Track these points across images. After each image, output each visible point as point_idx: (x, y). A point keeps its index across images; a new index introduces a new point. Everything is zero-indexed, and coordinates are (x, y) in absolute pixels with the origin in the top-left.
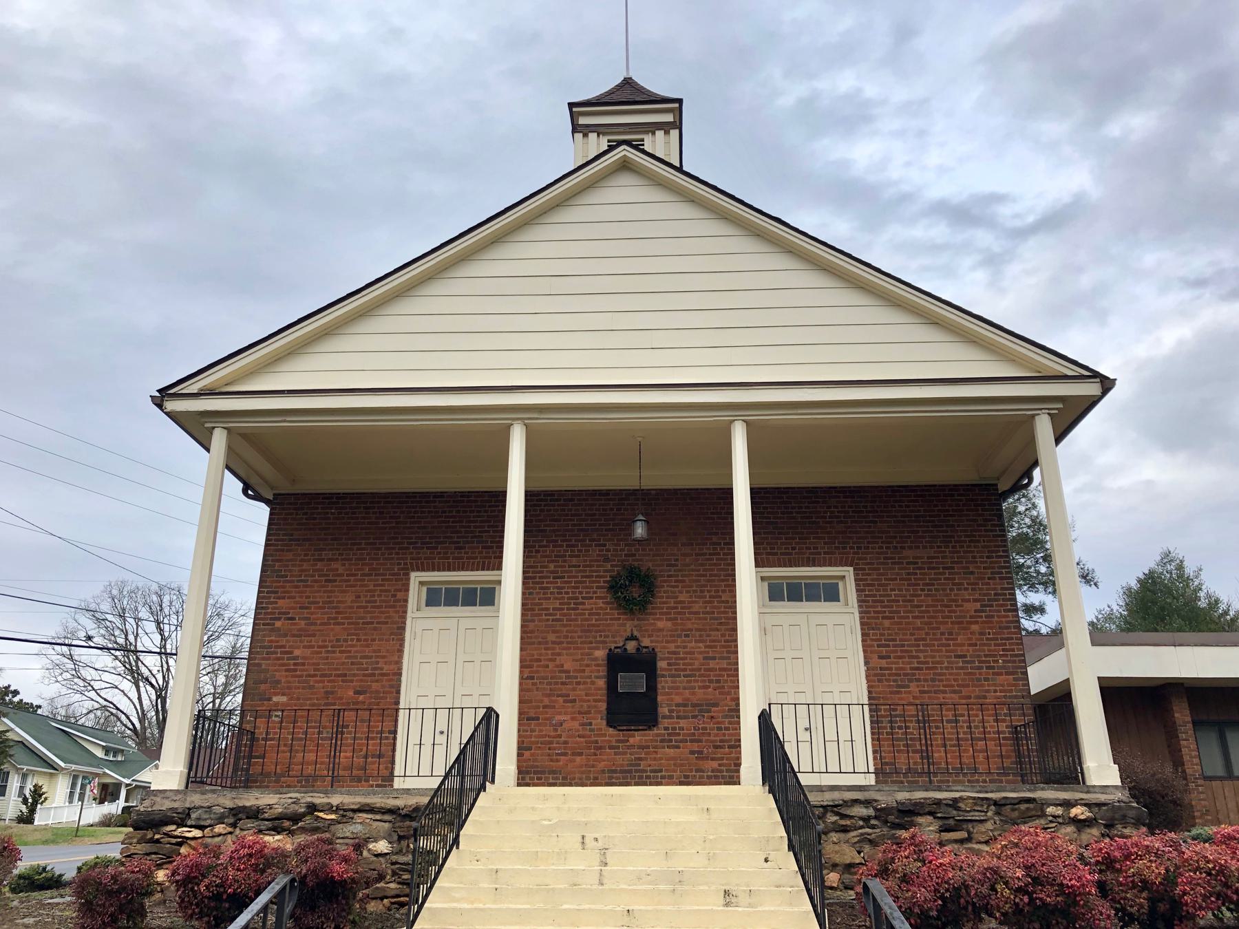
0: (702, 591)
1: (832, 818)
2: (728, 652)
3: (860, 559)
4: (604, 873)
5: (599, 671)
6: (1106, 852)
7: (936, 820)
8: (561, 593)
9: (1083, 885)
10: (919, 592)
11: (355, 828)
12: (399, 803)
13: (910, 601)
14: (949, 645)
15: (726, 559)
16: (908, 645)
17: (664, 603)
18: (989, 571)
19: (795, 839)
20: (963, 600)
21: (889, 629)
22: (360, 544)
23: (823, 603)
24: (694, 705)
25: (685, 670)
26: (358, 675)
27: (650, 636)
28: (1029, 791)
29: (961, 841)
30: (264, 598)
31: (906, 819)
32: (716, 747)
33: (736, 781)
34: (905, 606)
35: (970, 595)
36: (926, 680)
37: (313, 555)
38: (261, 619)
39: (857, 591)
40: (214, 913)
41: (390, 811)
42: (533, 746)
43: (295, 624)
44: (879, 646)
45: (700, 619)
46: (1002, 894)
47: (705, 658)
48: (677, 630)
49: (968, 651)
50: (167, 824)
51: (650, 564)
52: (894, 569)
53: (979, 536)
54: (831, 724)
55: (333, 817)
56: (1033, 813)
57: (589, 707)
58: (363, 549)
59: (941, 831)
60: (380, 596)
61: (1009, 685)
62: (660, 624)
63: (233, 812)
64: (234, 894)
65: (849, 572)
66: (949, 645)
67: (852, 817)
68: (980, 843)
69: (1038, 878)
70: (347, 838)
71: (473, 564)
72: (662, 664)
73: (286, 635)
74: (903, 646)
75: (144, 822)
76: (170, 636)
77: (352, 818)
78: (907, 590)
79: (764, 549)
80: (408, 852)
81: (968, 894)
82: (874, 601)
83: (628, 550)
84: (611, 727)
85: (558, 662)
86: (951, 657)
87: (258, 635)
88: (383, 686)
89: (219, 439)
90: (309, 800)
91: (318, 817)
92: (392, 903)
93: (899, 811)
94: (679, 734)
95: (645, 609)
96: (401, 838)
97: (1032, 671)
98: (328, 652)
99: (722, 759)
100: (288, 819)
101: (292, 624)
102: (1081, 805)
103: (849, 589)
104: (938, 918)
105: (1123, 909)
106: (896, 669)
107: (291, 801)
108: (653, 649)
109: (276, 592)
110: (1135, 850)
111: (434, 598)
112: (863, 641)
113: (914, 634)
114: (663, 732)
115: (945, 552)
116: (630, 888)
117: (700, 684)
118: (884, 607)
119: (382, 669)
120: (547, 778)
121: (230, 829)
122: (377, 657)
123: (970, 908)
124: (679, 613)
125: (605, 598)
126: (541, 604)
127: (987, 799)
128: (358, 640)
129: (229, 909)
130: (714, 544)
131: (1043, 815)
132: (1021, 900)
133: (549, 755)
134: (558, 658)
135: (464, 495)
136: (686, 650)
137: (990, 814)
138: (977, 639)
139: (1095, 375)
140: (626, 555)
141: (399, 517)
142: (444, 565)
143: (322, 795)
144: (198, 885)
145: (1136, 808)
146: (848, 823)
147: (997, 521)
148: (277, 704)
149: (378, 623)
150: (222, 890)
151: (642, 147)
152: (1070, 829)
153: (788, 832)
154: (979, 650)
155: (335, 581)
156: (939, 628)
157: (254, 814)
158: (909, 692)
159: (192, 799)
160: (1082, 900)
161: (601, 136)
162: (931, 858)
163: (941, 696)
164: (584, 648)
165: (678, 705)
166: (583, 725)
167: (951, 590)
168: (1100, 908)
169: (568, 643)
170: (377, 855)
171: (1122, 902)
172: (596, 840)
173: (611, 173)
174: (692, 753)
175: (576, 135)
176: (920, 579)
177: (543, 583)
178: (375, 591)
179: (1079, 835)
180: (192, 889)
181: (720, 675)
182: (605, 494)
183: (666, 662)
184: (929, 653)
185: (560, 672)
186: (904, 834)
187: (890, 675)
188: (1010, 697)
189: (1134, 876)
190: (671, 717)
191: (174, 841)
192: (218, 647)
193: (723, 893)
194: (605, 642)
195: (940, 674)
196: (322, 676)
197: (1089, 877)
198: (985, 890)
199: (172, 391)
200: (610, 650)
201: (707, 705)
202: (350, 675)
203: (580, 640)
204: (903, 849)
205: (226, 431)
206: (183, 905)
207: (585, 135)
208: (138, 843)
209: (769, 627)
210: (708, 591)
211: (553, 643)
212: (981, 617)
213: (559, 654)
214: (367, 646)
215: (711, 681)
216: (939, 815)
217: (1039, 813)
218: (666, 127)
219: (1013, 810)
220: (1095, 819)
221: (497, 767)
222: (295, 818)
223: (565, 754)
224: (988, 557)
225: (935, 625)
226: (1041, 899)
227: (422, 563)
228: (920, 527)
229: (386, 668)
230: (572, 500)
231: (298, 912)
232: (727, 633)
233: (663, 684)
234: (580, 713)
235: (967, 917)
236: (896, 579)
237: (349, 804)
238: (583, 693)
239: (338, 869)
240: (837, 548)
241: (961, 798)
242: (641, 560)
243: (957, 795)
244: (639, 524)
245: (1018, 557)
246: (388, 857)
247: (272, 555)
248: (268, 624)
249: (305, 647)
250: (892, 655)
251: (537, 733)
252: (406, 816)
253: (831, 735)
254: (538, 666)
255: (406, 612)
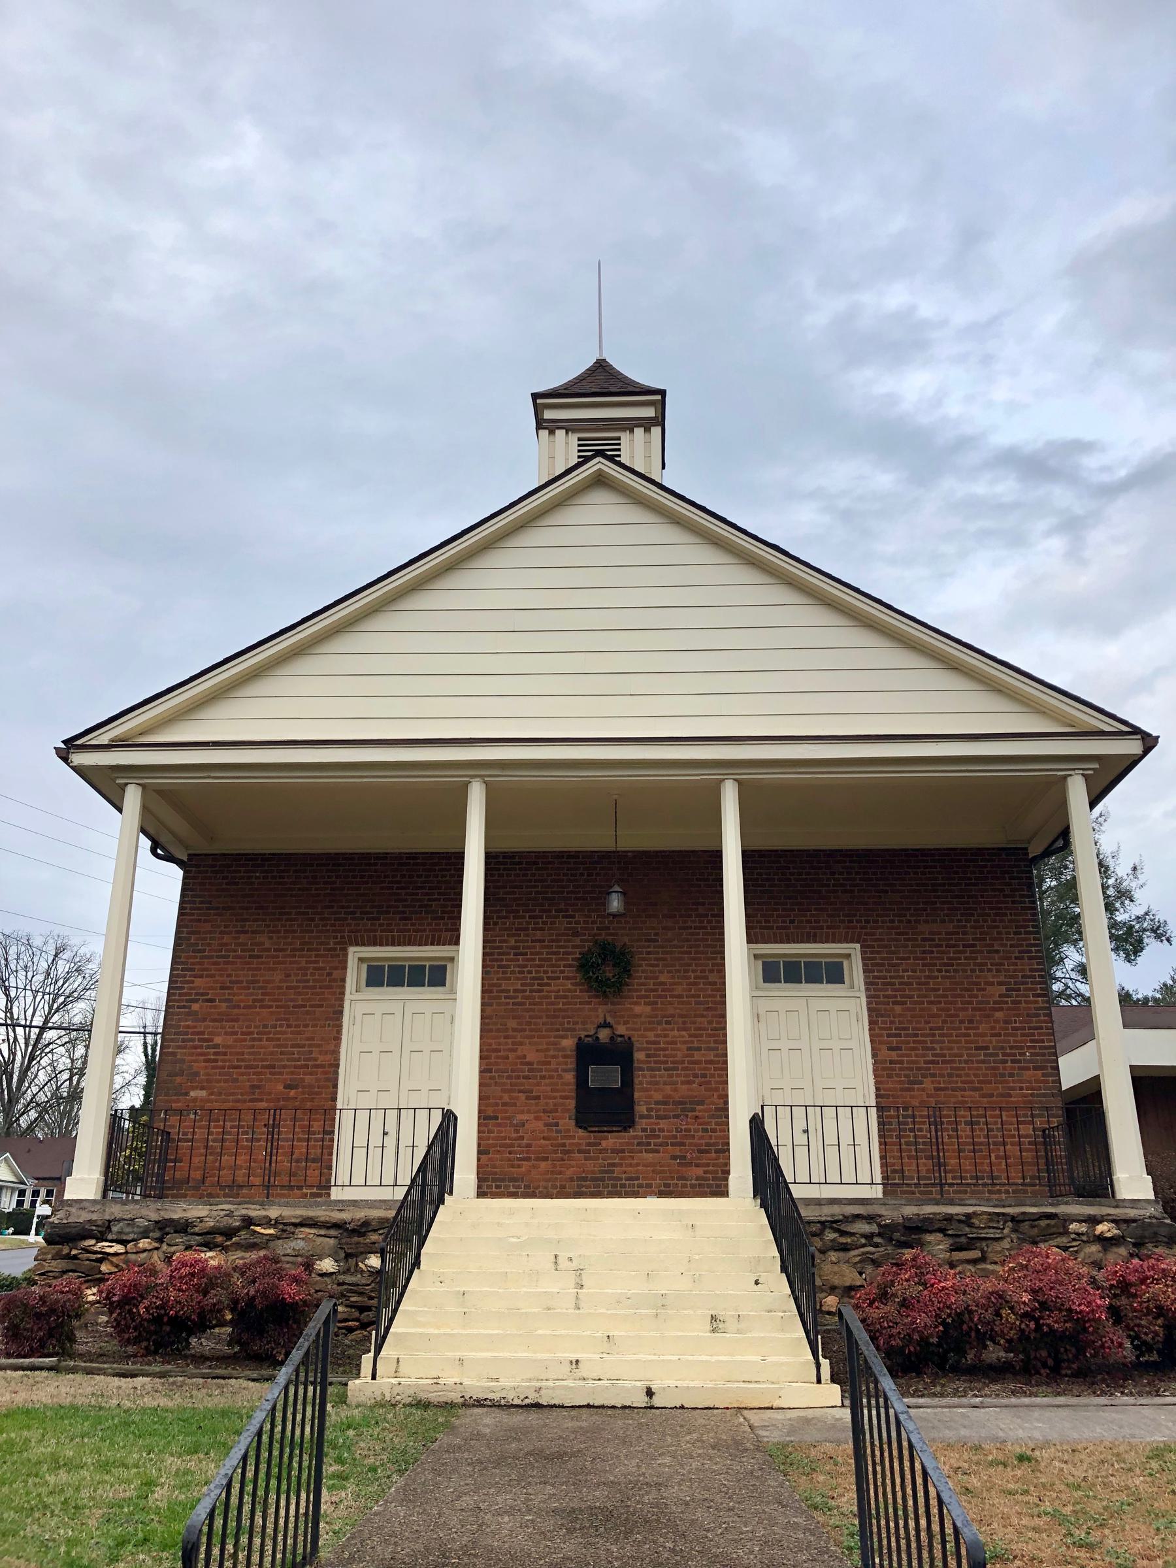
0: (686, 971)
1: (830, 1235)
2: (715, 1042)
3: (866, 934)
4: (580, 1296)
5: (566, 1064)
6: (1121, 1275)
7: (947, 1238)
8: (523, 972)
9: (1093, 1310)
10: (936, 974)
11: (298, 1244)
12: (345, 1216)
13: (924, 984)
14: (969, 1035)
15: (714, 934)
16: (922, 1035)
17: (642, 984)
18: (1017, 949)
19: (788, 1259)
20: (987, 983)
21: (900, 1015)
22: (290, 914)
23: (825, 985)
24: (675, 1103)
25: (666, 1062)
26: (289, 1067)
27: (626, 1023)
28: (1052, 1205)
29: (974, 1262)
30: (178, 976)
31: (913, 1236)
32: (700, 1151)
33: (724, 1193)
34: (920, 990)
35: (994, 977)
36: (942, 1076)
37: (235, 926)
38: (174, 1001)
39: (865, 971)
40: (154, 1337)
41: (336, 1226)
42: (492, 1150)
43: (215, 1007)
44: (889, 1036)
45: (683, 1003)
46: (1007, 1320)
47: (689, 1049)
48: (656, 1016)
49: (991, 1042)
50: (85, 1238)
51: (626, 939)
52: (907, 946)
53: (1005, 908)
54: (830, 1125)
55: (271, 1231)
56: (1054, 1230)
57: (555, 1105)
58: (294, 920)
59: (952, 1250)
60: (312, 974)
61: (1037, 1081)
62: (638, 1009)
63: (159, 1225)
64: (176, 1316)
65: (855, 949)
66: (969, 1035)
67: (852, 1234)
68: (996, 1263)
69: (1045, 1303)
70: (288, 1255)
71: (421, 937)
72: (639, 1056)
73: (204, 1020)
74: (916, 1035)
75: (59, 1236)
76: (17, 997)
77: (293, 1233)
78: (922, 971)
79: (759, 922)
80: (356, 1271)
81: (971, 1320)
82: (883, 984)
83: (601, 923)
84: (580, 1127)
85: (519, 1053)
86: (970, 1049)
87: (172, 1019)
88: (318, 1080)
89: (133, 797)
90: (244, 1212)
91: (255, 1231)
92: (340, 1328)
93: (906, 1228)
94: (659, 1137)
95: (620, 990)
96: (348, 1256)
97: (1063, 1061)
98: (254, 1040)
99: (708, 1165)
100: (221, 1234)
101: (211, 1007)
102: (1108, 1221)
103: (855, 970)
104: (939, 1345)
105: (1137, 1337)
106: (908, 1062)
107: (222, 1213)
108: (629, 1038)
109: (192, 970)
110: (1152, 1273)
111: (377, 977)
112: (870, 1030)
113: (929, 1023)
114: (640, 1134)
115: (965, 927)
116: (609, 1312)
117: (683, 1079)
118: (896, 990)
119: (316, 1060)
120: (507, 1187)
121: (157, 1245)
122: (310, 1046)
123: (973, 1334)
124: (660, 997)
125: (575, 978)
126: (500, 985)
127: (1004, 1214)
128: (289, 1026)
129: (168, 1334)
130: (701, 916)
131: (1066, 1232)
132: (1027, 1326)
133: (509, 1160)
134: (520, 1048)
135: (413, 856)
136: (667, 1039)
137: (1006, 1231)
138: (1001, 1028)
139: (1136, 731)
140: (598, 929)
141: (335, 883)
142: (387, 940)
143: (258, 1207)
144: (137, 1307)
145: (1168, 1224)
146: (849, 1240)
147: (1029, 887)
148: (195, 1100)
149: (311, 1006)
150: (162, 1312)
151: (617, 459)
152: (1094, 1248)
153: (780, 1251)
154: (1004, 1041)
155: (261, 957)
156: (958, 1016)
157: (183, 1227)
158: (923, 1090)
159: (113, 1210)
160: (1091, 1326)
161: (570, 433)
162: (933, 1281)
163: (959, 1093)
164: (549, 1037)
165: (657, 1103)
166: (546, 1125)
167: (973, 971)
168: (1111, 1335)
169: (531, 1030)
170: (323, 1275)
171: (1136, 1329)
172: (570, 1259)
173: (589, 486)
174: (674, 1158)
175: (541, 432)
176: (937, 958)
177: (502, 960)
178: (308, 969)
179: (1105, 1254)
180: (130, 1311)
181: (705, 1069)
182: (576, 855)
183: (644, 1053)
184: (946, 1044)
185: (522, 1064)
186: (908, 1254)
187: (901, 1069)
188: (1038, 1095)
189: (1149, 1301)
190: (649, 1117)
191: (94, 1257)
192: (76, 1011)
193: (709, 1318)
194: (574, 1030)
195: (958, 1069)
196: (247, 1067)
197: (1099, 1302)
198: (989, 1316)
199: (79, 742)
200: (580, 1039)
201: (691, 1103)
202: (279, 1067)
203: (544, 1027)
204: (903, 1271)
205: (140, 789)
206: (120, 1328)
207: (552, 432)
208: (53, 1259)
209: (762, 1012)
210: (693, 971)
211: (514, 1030)
212: (1007, 1003)
213: (521, 1044)
214: (299, 1033)
215: (695, 1076)
216: (950, 1232)
217: (1061, 1230)
218: (646, 424)
219: (1033, 1227)
220: (1123, 1237)
221: (456, 1176)
222: (229, 1233)
223: (527, 1159)
224: (1015, 933)
225: (952, 1012)
226: (1048, 1325)
227: (362, 937)
228: (938, 897)
229: (321, 1059)
230: (535, 863)
231: (245, 1337)
232: (715, 1019)
233: (641, 1079)
234: (545, 1111)
235: (970, 1343)
236: (909, 958)
237: (290, 1217)
238: (549, 1088)
239: (290, 1291)
240: (842, 921)
241: (974, 1213)
242: (616, 934)
243: (970, 1210)
244: (614, 896)
245: (1072, 905)
246: (334, 1277)
247: (187, 927)
248: (184, 1007)
249: (226, 1034)
250: (903, 1046)
251: (495, 1135)
252: (353, 1231)
253: (831, 1138)
254: (497, 1057)
255: (343, 993)
